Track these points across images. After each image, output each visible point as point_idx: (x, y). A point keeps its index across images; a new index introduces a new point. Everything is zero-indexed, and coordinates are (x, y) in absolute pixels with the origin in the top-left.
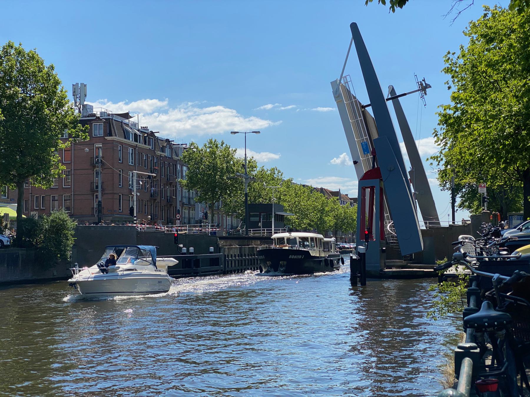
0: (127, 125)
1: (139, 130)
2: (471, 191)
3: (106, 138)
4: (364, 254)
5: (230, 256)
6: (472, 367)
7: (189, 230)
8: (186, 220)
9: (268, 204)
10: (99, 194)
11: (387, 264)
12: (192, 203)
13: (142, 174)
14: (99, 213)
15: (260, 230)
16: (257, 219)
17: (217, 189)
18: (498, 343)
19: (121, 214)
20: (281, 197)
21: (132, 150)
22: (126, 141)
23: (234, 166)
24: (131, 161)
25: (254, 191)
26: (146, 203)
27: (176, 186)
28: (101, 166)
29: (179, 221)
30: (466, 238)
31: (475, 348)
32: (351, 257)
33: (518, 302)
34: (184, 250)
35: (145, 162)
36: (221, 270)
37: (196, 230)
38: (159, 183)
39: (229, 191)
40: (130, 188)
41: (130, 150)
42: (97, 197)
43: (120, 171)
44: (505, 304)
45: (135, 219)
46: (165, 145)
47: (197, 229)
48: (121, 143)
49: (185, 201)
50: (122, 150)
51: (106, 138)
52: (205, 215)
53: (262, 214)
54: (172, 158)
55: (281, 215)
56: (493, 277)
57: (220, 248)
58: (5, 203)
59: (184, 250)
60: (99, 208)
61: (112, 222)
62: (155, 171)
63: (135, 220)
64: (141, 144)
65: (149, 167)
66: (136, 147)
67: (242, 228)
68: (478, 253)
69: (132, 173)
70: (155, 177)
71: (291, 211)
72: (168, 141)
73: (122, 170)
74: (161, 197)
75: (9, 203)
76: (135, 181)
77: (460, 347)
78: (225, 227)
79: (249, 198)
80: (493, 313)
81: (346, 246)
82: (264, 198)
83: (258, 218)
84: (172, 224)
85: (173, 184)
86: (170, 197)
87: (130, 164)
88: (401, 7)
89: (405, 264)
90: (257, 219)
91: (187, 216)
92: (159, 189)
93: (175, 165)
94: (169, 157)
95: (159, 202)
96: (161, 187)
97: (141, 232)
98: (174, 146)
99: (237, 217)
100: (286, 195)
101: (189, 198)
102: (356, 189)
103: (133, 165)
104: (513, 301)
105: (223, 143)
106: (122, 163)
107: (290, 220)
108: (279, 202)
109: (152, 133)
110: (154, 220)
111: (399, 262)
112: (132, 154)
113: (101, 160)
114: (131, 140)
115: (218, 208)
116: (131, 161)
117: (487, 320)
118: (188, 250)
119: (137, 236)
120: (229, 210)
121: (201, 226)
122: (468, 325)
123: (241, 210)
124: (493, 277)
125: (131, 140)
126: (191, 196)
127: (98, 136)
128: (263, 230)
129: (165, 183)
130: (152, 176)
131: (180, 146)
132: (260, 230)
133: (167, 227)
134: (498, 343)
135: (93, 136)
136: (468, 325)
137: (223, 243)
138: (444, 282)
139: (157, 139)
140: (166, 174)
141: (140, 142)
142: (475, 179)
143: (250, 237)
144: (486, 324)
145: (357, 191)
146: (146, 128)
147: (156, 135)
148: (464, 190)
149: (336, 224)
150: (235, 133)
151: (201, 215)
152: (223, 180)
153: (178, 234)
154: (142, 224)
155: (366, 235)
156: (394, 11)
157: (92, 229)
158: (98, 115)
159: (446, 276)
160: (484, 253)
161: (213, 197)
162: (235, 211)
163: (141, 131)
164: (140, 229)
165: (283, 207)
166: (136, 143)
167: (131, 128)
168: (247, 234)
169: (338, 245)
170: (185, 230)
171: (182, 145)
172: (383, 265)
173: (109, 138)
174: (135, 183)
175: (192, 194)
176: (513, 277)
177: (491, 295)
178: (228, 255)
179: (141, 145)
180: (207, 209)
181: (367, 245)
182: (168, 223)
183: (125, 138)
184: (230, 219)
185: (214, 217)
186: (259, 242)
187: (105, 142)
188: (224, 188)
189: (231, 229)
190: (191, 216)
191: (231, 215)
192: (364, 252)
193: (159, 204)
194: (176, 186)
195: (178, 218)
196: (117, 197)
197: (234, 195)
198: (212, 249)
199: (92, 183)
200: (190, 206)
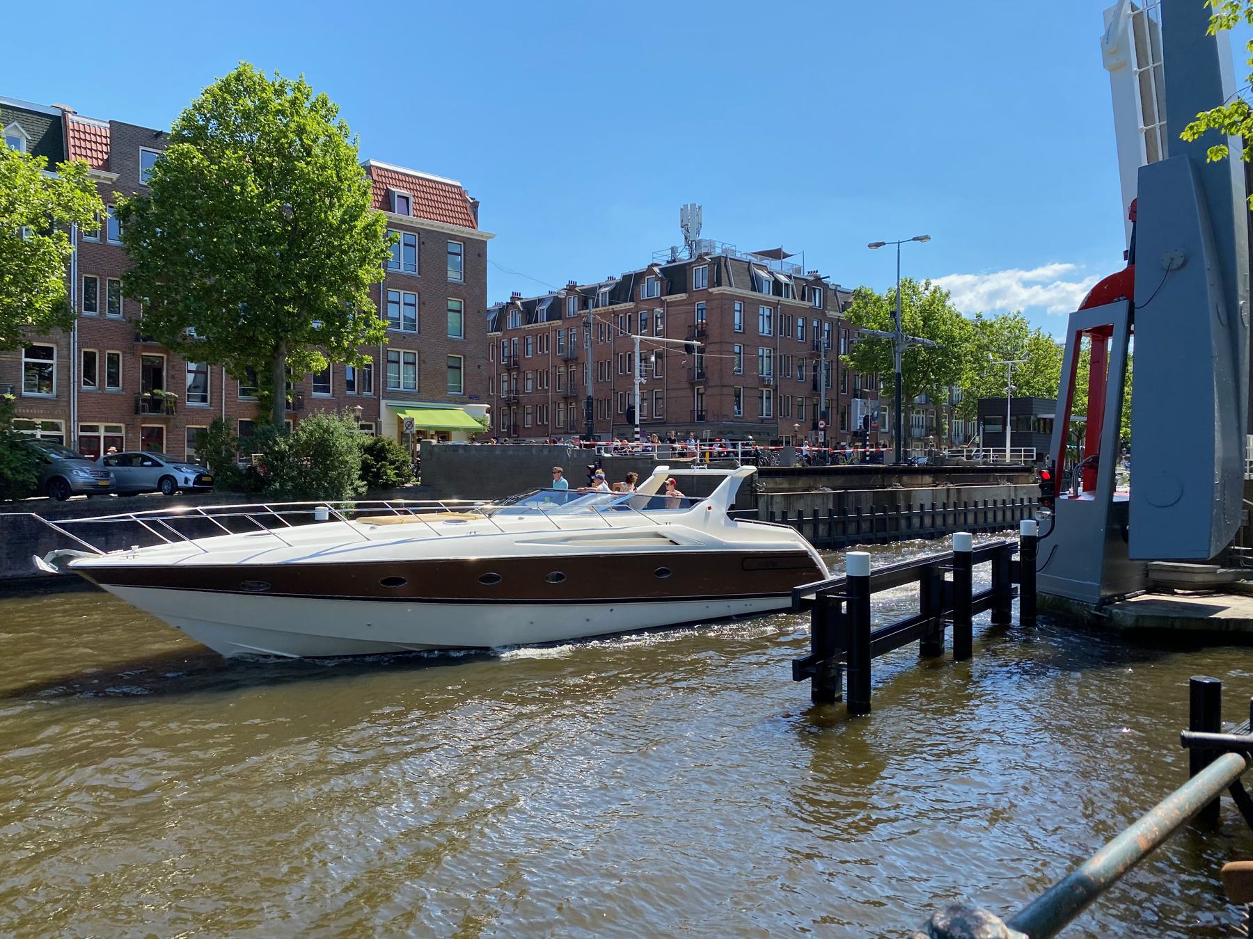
3: (710, 290)
11: (1154, 576)
22: (755, 295)
58: (455, 403)
89: (1229, 578)
111: (1208, 572)
150: (878, 245)
166: (777, 298)
173: (715, 290)
183: (754, 289)
187: (710, 298)
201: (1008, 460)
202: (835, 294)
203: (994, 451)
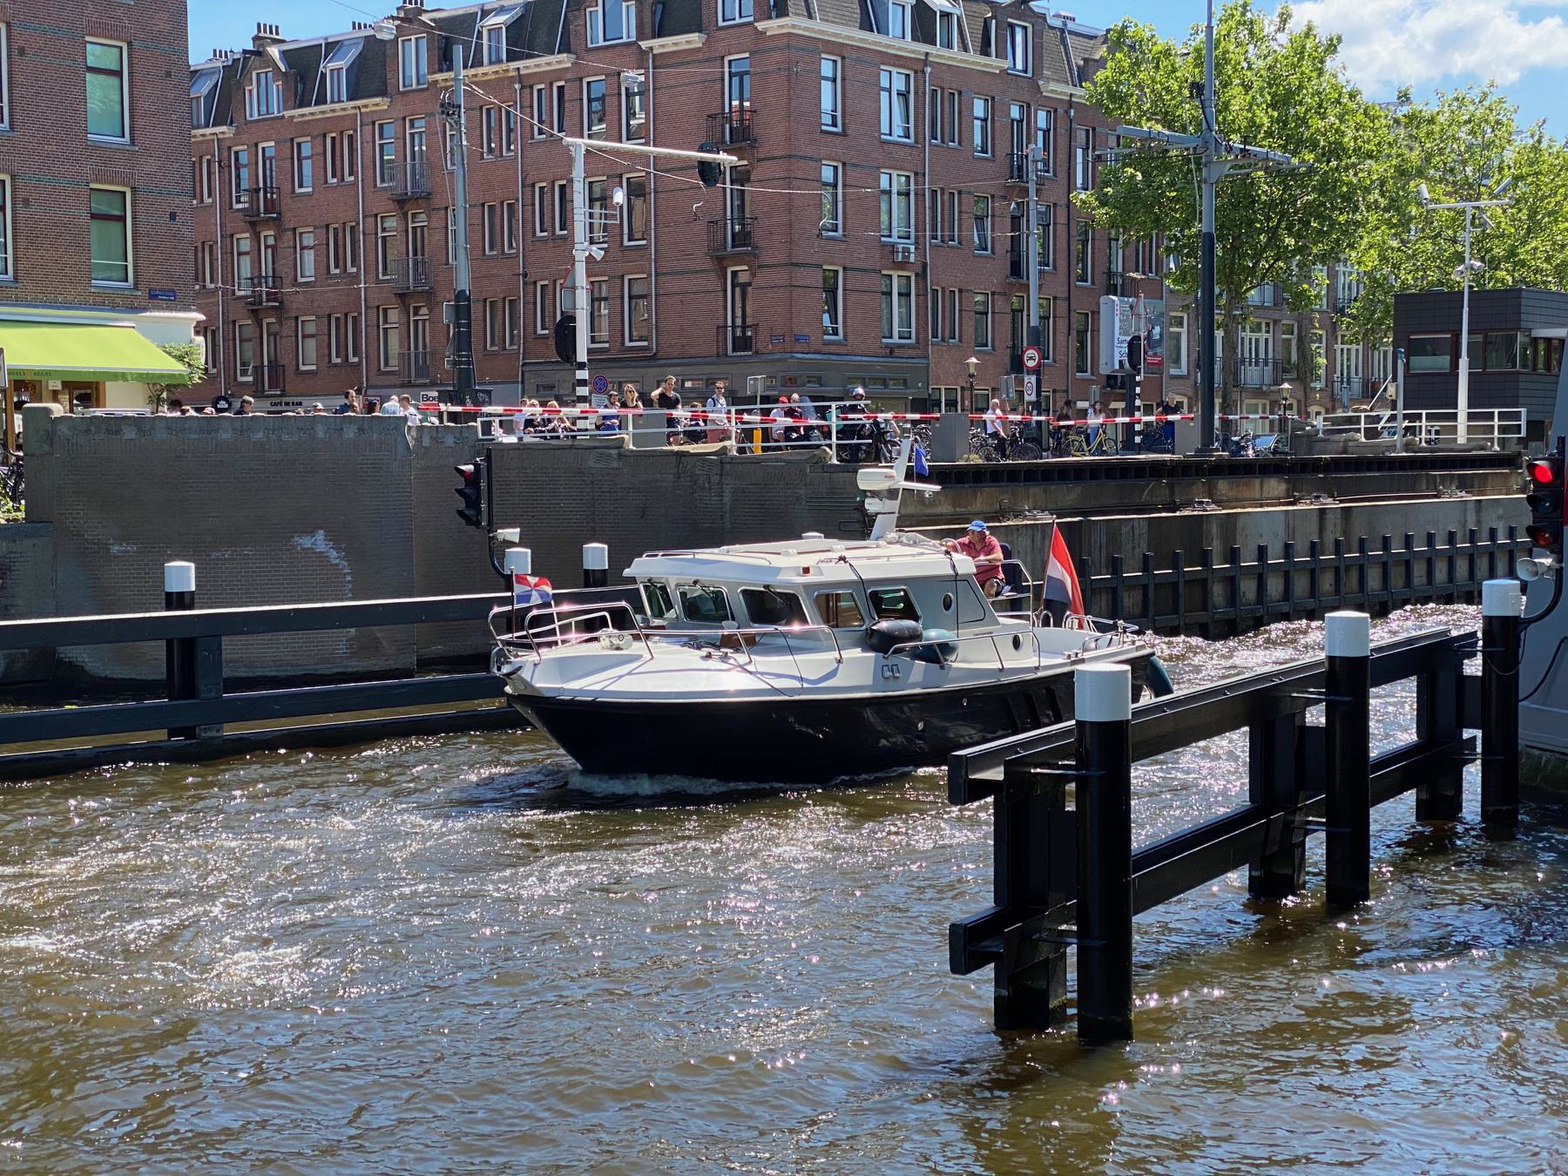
3: (760, 26)
66: (925, 62)
75: (134, 309)
103: (911, 141)
127: (738, 21)
135: (721, 23)
166: (923, 48)
173: (772, 26)
183: (866, 25)
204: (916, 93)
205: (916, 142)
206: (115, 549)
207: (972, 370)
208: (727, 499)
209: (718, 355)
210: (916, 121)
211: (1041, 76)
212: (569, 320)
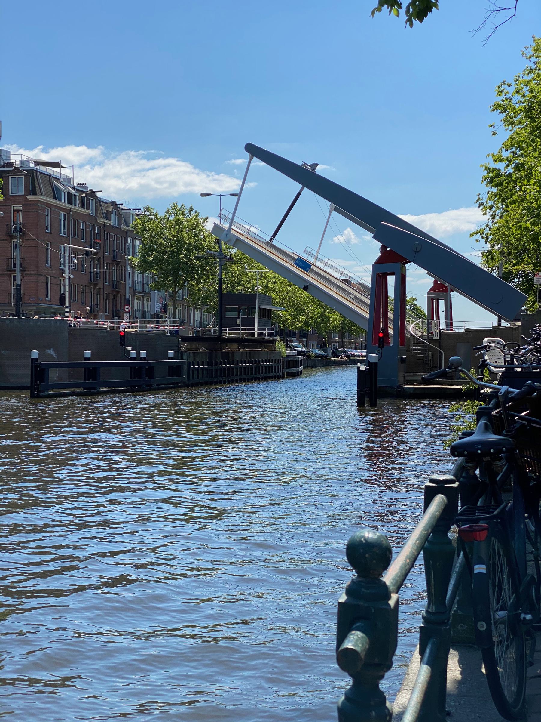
0: (58, 180)
1: (74, 188)
2: (526, 282)
3: (28, 197)
4: (377, 363)
5: (196, 363)
6: (443, 507)
7: (141, 327)
8: (139, 314)
9: (250, 295)
10: (18, 275)
11: (407, 378)
12: (147, 290)
13: (77, 248)
14: (17, 301)
15: (239, 329)
16: (235, 314)
17: (181, 273)
18: (498, 479)
19: (48, 303)
20: (269, 285)
21: (64, 215)
23: (205, 242)
24: (62, 230)
25: (232, 276)
26: (83, 289)
27: (125, 267)
28: (20, 236)
29: (128, 315)
30: (494, 342)
31: (451, 482)
32: (359, 368)
33: (533, 425)
34: (134, 354)
35: (82, 233)
36: (184, 383)
37: (152, 328)
38: (102, 262)
39: (198, 275)
40: (62, 268)
41: (62, 215)
42: (15, 280)
43: (47, 244)
44: (514, 427)
45: (67, 310)
46: (110, 210)
47: (153, 326)
48: (50, 206)
49: (138, 287)
50: (51, 215)
51: (28, 197)
52: (163, 308)
53: (243, 308)
54: (119, 228)
55: (266, 309)
56: (500, 389)
57: (182, 353)
59: (134, 354)
60: (17, 294)
61: (36, 313)
62: (95, 244)
63: (67, 312)
64: (76, 208)
65: (88, 239)
66: (70, 211)
67: (214, 326)
68: (508, 361)
69: (64, 247)
70: (96, 254)
71: (282, 304)
72: (114, 204)
73: (51, 243)
74: (105, 281)
76: (67, 258)
77: (432, 481)
78: (192, 324)
79: (223, 287)
80: (493, 437)
81: (356, 354)
82: (246, 285)
83: (236, 313)
84: (119, 319)
85: (121, 264)
86: (117, 282)
87: (62, 235)
88: (421, 20)
90: (235, 314)
91: (139, 307)
92: (102, 270)
93: (125, 238)
94: (115, 227)
95: (102, 287)
96: (104, 268)
97: (75, 329)
98: (123, 211)
99: (207, 311)
100: (275, 283)
101: (143, 284)
102: (369, 277)
104: (526, 423)
105: (191, 210)
106: (51, 233)
107: (280, 317)
108: (266, 292)
109: (93, 193)
110: (94, 312)
112: (64, 221)
113: (20, 228)
114: (63, 201)
115: (183, 298)
116: (62, 230)
117: (480, 446)
118: (138, 354)
119: (69, 334)
120: (198, 301)
121: (158, 322)
122: (456, 453)
123: (214, 302)
124: (500, 389)
125: (63, 201)
126: (146, 280)
127: (17, 194)
128: (242, 329)
129: (110, 262)
130: (91, 252)
131: (131, 211)
132: (239, 329)
133: (111, 322)
134: (498, 479)
135: (10, 194)
136: (456, 453)
137: (187, 346)
138: (469, 401)
139: (99, 201)
140: (111, 249)
141: (75, 205)
142: (531, 265)
143: (225, 338)
144: (479, 451)
145: (370, 279)
146: (83, 185)
147: (98, 195)
148: (516, 280)
149: (343, 323)
151: (158, 307)
152: (189, 260)
153: (125, 332)
154: (77, 317)
155: (380, 338)
156: (411, 25)
157: (7, 322)
158: (17, 165)
159: (484, 396)
160: (515, 360)
161: (176, 282)
162: (206, 303)
163: (77, 190)
164: (74, 324)
165: (271, 298)
166: (70, 206)
167: (63, 185)
168: (220, 334)
169: (345, 352)
170: (136, 327)
171: (134, 210)
172: (401, 379)
173: (31, 197)
174: (67, 261)
175: (146, 278)
176: (523, 389)
177: (498, 415)
178: (193, 362)
179: (77, 208)
180: (167, 300)
181: (382, 352)
182: (113, 318)
183: (55, 198)
184: (199, 313)
185: (177, 311)
186: (236, 346)
187: (26, 203)
188: (190, 269)
189: (200, 327)
190: (146, 309)
191: (199, 308)
192: (376, 361)
193: (102, 290)
194: (125, 267)
195: (127, 310)
196: (42, 279)
197: (205, 282)
198: (171, 353)
199: (9, 259)
200: (144, 294)
201: (256, 336)
202: (100, 204)
203: (229, 330)
204: (68, 220)
205: (68, 236)
206: (3, 352)
207: (88, 311)
208: (138, 343)
209: (8, 303)
210: (68, 229)
211: (97, 216)
212: (64, 294)
